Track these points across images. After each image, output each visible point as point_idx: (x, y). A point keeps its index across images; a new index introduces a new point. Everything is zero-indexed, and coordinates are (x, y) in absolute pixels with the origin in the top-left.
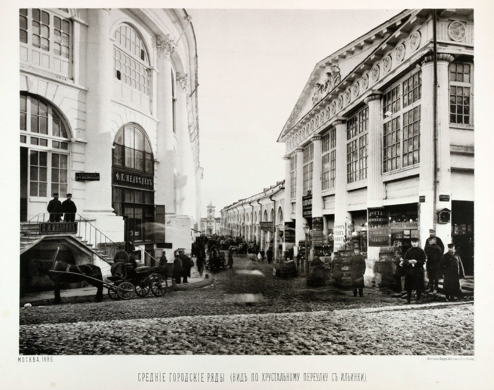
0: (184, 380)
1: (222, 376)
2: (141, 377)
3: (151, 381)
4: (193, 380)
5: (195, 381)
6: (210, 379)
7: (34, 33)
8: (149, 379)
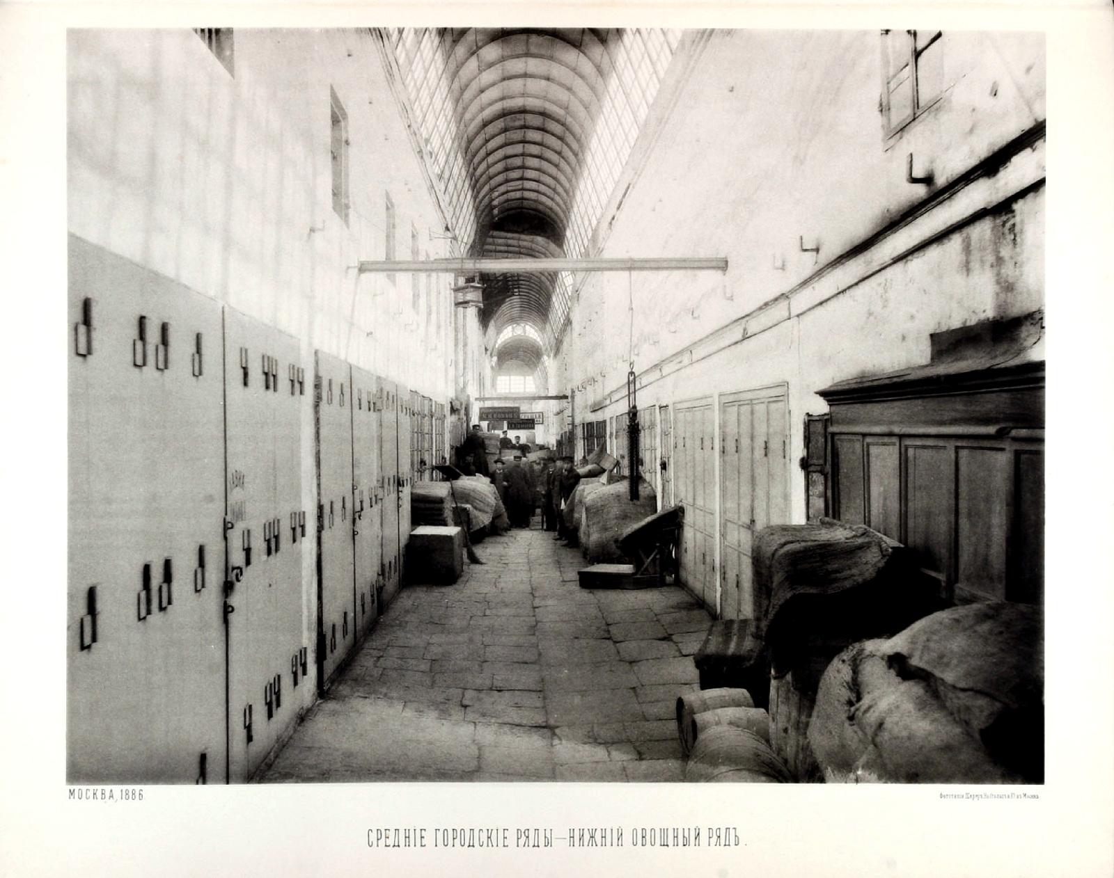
0: (467, 844)
1: (548, 835)
2: (373, 836)
3: (394, 846)
4: (485, 844)
5: (594, 844)
6: (522, 841)
7: (263, 384)
8: (390, 842)
